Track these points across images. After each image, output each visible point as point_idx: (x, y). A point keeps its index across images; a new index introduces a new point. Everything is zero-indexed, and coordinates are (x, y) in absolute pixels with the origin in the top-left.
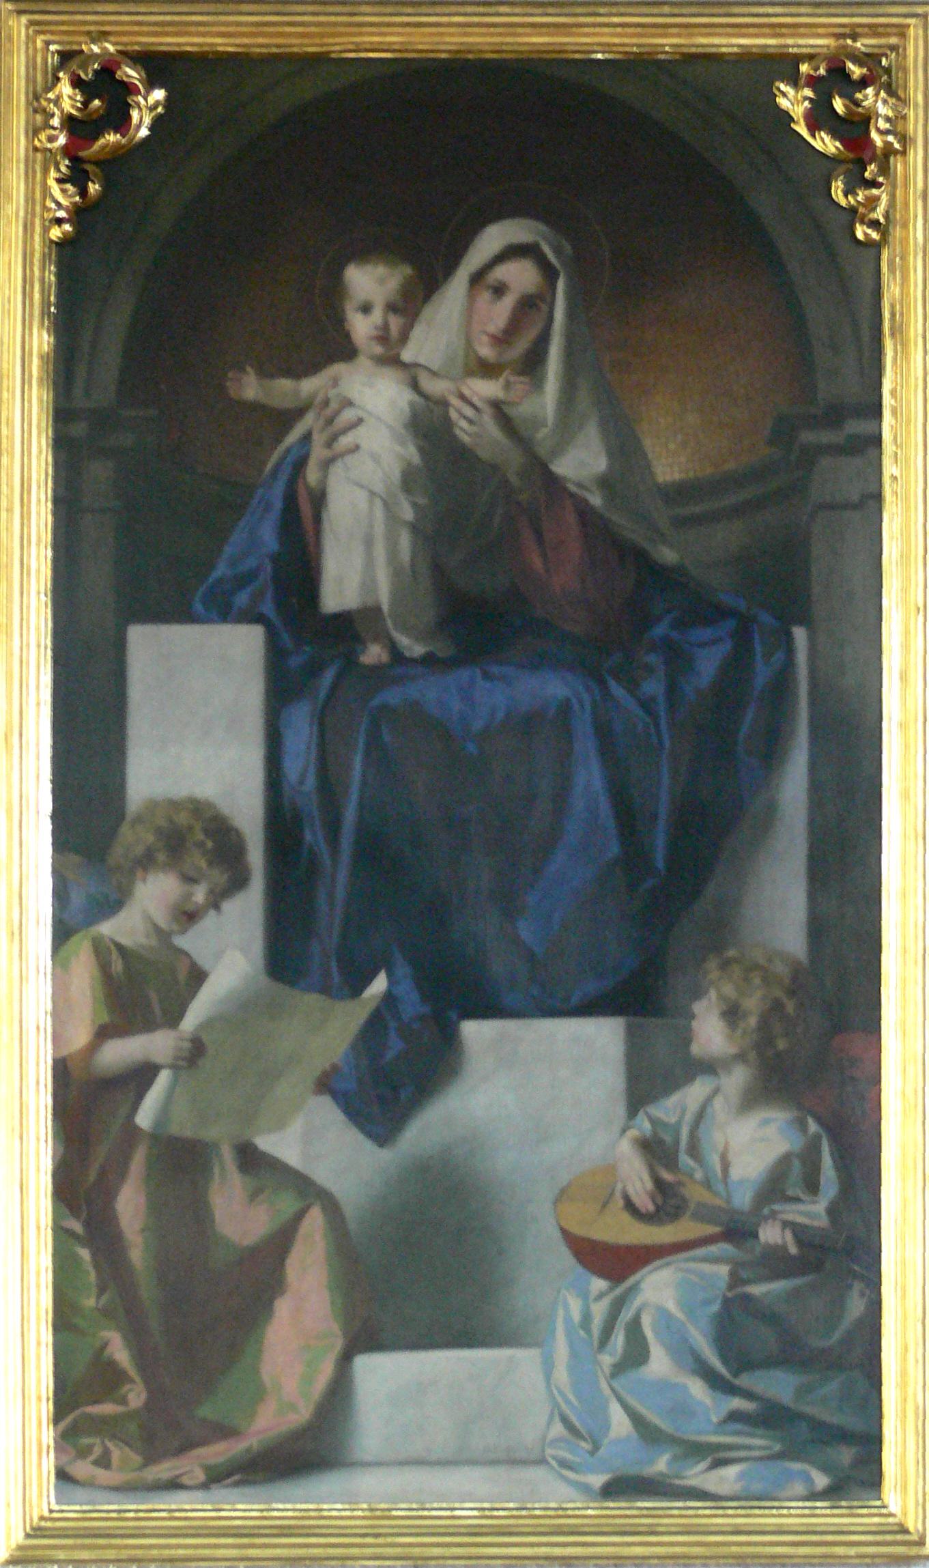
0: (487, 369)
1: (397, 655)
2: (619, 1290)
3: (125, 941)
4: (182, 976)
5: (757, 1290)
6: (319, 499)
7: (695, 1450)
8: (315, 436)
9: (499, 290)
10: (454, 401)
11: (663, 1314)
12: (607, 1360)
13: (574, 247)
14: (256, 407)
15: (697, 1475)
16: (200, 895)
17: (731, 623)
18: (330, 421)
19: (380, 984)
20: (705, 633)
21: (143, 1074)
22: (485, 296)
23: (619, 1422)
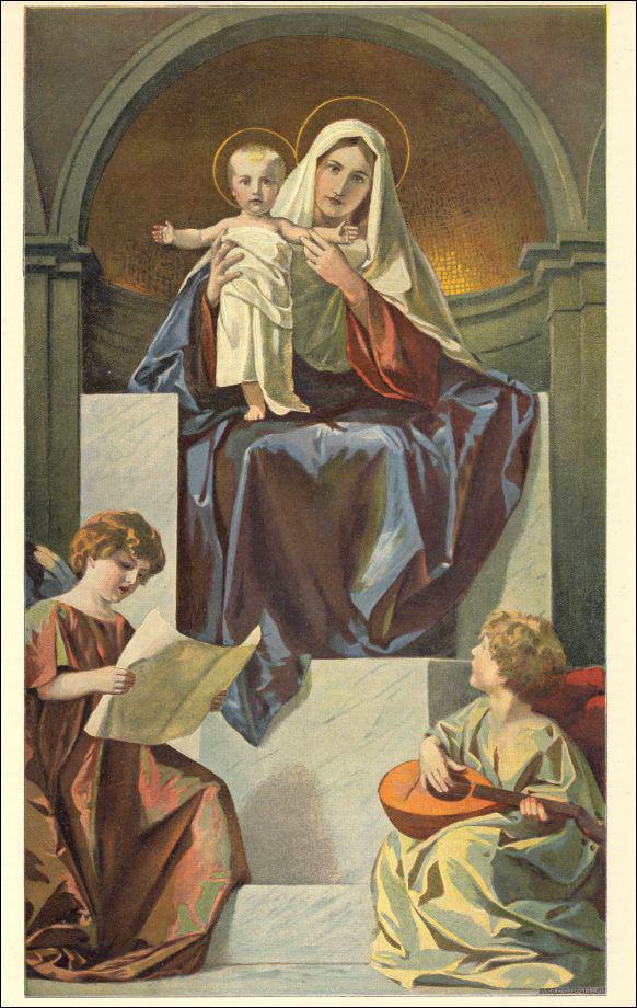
0: (330, 222)
1: (269, 415)
2: (425, 844)
3: (79, 607)
4: (120, 629)
5: (519, 845)
6: (215, 311)
7: (477, 957)
8: (213, 266)
9: (337, 168)
10: (307, 243)
11: (452, 864)
12: (414, 896)
13: (387, 140)
14: (171, 247)
15: (476, 974)
16: (132, 576)
17: (496, 392)
18: (223, 257)
19: (255, 637)
20: (481, 397)
21: (90, 700)
22: (327, 173)
23: (427, 942)
